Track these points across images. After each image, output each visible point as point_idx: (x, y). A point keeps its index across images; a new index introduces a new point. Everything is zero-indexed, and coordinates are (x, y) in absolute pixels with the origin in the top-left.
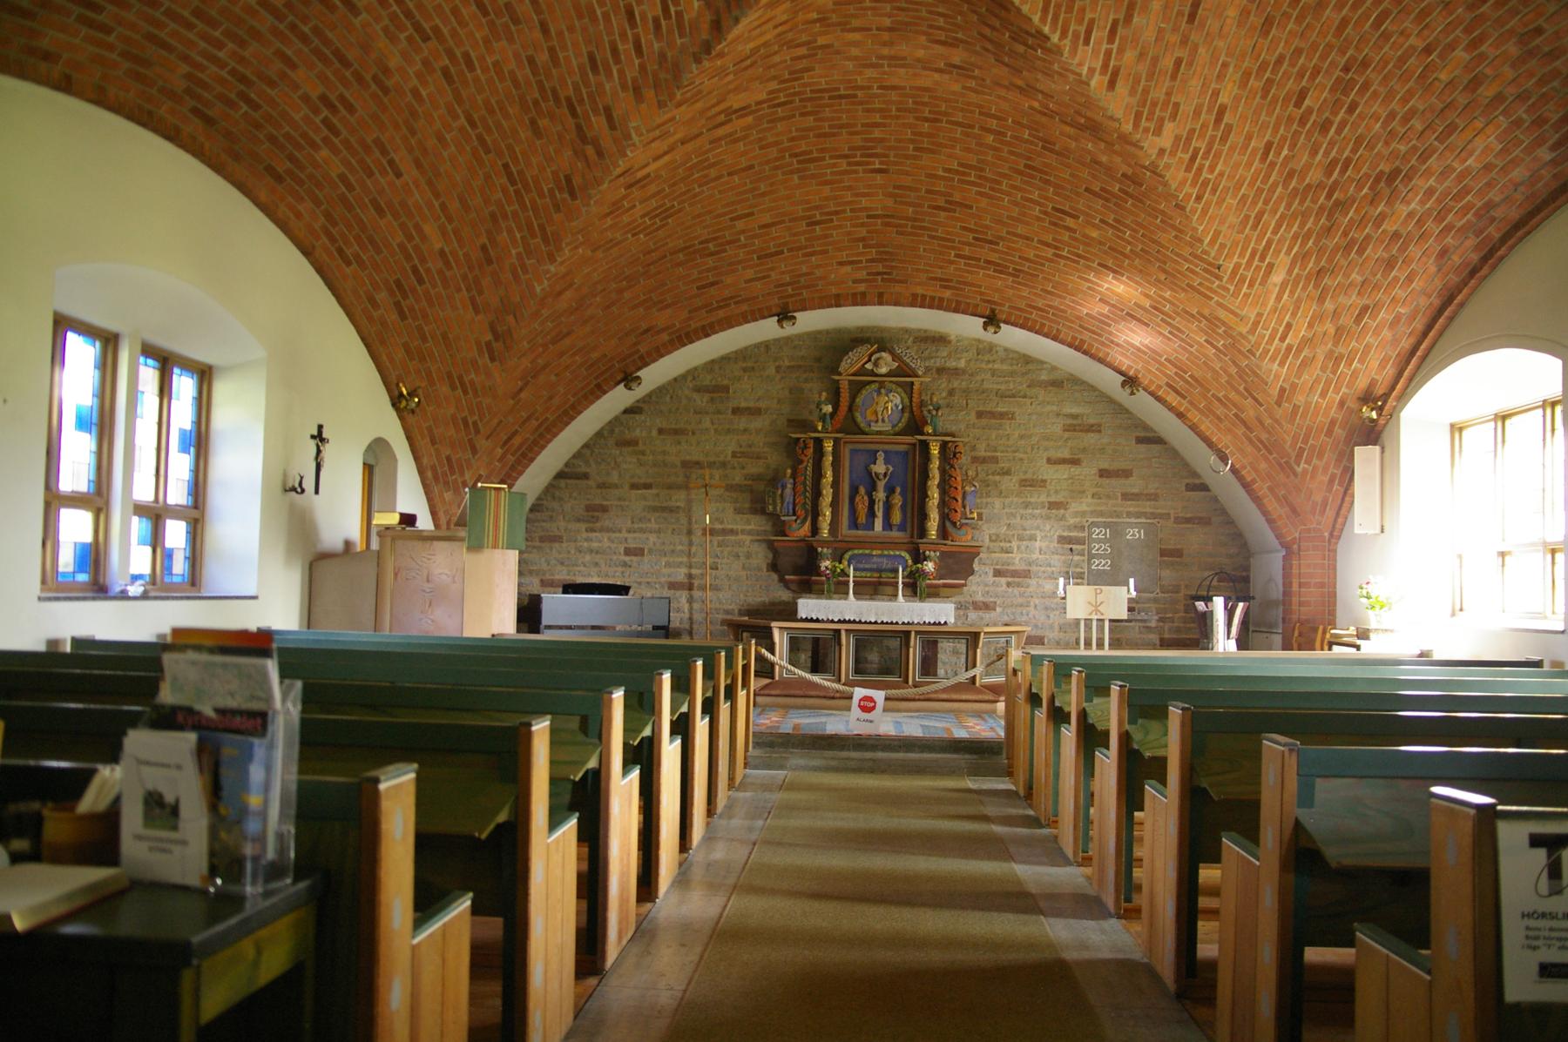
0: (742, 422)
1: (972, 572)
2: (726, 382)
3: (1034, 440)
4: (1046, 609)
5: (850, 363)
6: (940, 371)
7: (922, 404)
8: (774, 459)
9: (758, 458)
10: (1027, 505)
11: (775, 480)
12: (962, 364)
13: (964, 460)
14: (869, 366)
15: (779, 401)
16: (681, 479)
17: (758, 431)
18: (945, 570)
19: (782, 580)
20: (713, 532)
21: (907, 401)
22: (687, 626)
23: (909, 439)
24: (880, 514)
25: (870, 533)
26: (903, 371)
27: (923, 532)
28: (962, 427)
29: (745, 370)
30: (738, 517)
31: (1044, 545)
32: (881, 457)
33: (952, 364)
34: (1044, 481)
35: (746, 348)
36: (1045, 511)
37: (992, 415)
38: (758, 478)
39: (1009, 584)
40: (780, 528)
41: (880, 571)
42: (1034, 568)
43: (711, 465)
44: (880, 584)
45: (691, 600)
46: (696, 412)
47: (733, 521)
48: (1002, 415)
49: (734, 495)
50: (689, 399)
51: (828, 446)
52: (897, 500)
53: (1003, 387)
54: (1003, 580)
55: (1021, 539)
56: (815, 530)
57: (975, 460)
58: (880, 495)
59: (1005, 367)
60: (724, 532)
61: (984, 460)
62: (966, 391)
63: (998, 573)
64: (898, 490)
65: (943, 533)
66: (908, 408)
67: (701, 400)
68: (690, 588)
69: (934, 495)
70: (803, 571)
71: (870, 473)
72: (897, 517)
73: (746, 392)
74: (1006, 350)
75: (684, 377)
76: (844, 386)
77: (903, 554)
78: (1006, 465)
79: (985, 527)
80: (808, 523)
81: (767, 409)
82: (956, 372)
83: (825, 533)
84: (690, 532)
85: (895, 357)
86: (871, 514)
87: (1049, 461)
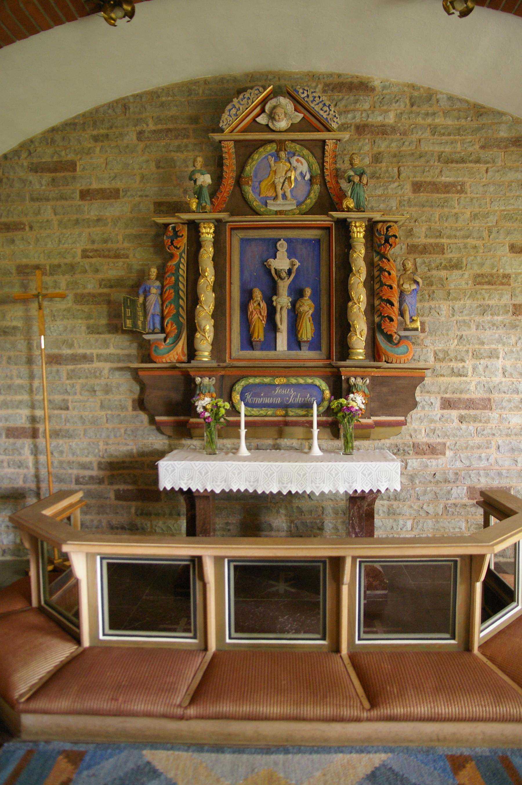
0: (93, 210)
1: (414, 405)
2: (71, 157)
3: (492, 220)
4: (513, 450)
5: (233, 120)
6: (361, 129)
7: (338, 174)
8: (139, 256)
9: (117, 256)
10: (484, 310)
11: (138, 285)
12: (391, 119)
13: (397, 251)
14: (262, 120)
15: (143, 178)
16: (16, 291)
17: (116, 221)
18: (380, 403)
19: (152, 421)
20: (54, 360)
21: (316, 167)
22: (33, 486)
23: (321, 219)
24: (283, 326)
25: (271, 354)
26: (312, 122)
27: (345, 351)
28: (394, 204)
29: (96, 139)
30: (92, 338)
31: (508, 364)
32: (282, 247)
33: (377, 119)
34: (507, 276)
35: (97, 110)
36: (508, 318)
37: (435, 187)
38: (116, 284)
39: (462, 419)
40: (146, 354)
41: (286, 406)
42: (496, 396)
43: (55, 269)
44: (287, 424)
45: (35, 451)
46: (32, 199)
47: (85, 343)
48: (447, 188)
49: (86, 308)
50: (24, 181)
51: (208, 233)
52: (307, 307)
53: (448, 149)
54: (454, 414)
55: (477, 355)
56: (192, 352)
57: (412, 249)
58: (283, 300)
59: (449, 122)
60: (76, 359)
61: (424, 250)
62: (398, 156)
63: (448, 404)
64: (308, 292)
65: (374, 352)
66: (319, 178)
67: (40, 183)
68: (34, 434)
69: (360, 295)
70: (176, 410)
71: (268, 271)
72: (307, 331)
73: (98, 168)
74: (450, 98)
75: (16, 153)
76: (229, 148)
77: (318, 382)
78: (454, 255)
79: (427, 342)
80: (183, 342)
81: (126, 191)
82: (383, 131)
83: (205, 354)
84: (30, 361)
85: (299, 104)
86: (272, 327)
87: (513, 248)
